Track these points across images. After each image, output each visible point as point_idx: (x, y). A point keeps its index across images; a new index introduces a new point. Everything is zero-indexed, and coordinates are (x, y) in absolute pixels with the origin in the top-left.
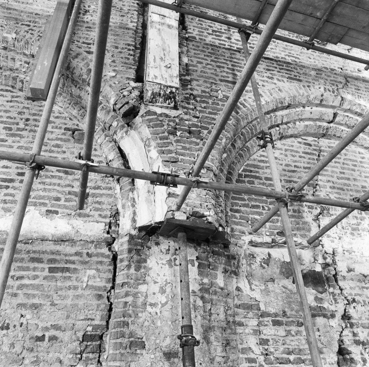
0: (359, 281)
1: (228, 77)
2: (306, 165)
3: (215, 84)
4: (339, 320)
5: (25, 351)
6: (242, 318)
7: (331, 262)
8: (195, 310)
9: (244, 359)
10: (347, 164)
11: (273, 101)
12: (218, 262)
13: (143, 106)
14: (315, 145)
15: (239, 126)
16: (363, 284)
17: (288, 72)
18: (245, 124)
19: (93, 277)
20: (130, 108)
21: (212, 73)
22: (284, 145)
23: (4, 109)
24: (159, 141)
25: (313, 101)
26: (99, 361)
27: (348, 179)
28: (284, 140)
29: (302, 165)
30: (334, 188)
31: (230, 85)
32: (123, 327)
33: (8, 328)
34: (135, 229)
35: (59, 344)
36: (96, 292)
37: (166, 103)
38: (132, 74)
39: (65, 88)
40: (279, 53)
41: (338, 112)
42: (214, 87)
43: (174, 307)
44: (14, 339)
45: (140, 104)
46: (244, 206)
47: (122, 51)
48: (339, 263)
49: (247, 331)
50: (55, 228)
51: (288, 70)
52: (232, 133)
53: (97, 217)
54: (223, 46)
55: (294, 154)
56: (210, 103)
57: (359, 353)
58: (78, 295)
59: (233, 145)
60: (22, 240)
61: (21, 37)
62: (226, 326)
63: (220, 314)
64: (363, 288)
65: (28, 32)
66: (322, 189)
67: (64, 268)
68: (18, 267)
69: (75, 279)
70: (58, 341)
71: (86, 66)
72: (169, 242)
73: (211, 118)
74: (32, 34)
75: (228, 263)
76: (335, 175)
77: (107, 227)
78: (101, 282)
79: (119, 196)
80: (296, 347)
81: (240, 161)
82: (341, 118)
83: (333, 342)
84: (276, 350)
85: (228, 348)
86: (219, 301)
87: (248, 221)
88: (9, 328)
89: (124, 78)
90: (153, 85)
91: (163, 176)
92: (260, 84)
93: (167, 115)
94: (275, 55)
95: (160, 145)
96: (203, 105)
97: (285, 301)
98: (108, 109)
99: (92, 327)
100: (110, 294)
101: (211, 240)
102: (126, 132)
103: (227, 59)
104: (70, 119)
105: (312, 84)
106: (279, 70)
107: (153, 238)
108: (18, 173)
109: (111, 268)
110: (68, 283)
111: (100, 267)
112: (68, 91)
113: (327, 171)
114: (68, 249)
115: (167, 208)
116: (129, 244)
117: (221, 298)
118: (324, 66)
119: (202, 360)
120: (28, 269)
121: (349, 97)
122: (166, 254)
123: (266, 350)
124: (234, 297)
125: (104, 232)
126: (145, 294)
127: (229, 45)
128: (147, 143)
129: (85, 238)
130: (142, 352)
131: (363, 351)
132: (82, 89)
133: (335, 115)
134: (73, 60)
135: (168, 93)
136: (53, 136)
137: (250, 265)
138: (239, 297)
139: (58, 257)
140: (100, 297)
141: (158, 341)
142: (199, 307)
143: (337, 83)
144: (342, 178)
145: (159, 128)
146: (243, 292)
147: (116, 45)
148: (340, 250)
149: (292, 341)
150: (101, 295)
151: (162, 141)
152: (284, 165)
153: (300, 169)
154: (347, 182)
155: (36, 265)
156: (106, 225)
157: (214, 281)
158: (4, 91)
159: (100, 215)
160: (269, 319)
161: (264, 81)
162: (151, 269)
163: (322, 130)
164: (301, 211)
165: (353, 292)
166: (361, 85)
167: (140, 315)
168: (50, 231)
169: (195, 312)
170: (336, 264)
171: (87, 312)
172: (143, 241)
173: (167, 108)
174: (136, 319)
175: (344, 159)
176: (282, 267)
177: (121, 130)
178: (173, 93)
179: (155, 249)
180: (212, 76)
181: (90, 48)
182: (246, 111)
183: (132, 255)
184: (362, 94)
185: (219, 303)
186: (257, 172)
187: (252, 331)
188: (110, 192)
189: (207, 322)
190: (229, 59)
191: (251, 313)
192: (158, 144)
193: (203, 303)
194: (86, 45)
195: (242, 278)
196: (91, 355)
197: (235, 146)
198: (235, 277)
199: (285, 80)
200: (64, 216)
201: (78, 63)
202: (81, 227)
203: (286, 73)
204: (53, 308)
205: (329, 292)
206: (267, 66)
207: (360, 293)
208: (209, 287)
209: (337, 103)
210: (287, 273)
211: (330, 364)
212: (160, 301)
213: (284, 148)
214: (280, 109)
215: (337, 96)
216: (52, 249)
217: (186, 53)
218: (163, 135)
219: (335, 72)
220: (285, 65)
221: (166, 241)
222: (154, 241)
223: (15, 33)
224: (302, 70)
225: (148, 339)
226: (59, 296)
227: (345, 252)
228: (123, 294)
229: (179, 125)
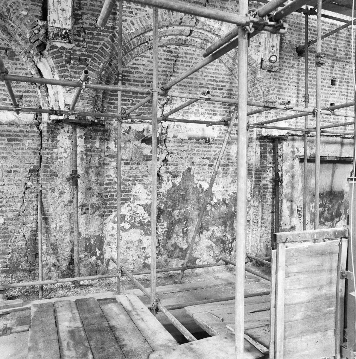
0: (179, 142)
2: (164, 69)
14: (175, 52)
16: (180, 144)
19: (31, 143)
24: (60, 69)
41: (194, 29)
52: (108, 58)
63: (96, 160)
75: (103, 135)
79: (40, 97)
82: (196, 34)
96: (90, 36)
102: (40, 59)
109: (40, 138)
110: (18, 147)
111: (33, 138)
133: (191, 32)
139: (11, 133)
140: (35, 153)
173: (64, 42)
176: (136, 134)
179: (61, 130)
186: (129, 76)
188: (35, 94)
192: (59, 71)
196: (34, 178)
209: (192, 24)
225: (59, 173)
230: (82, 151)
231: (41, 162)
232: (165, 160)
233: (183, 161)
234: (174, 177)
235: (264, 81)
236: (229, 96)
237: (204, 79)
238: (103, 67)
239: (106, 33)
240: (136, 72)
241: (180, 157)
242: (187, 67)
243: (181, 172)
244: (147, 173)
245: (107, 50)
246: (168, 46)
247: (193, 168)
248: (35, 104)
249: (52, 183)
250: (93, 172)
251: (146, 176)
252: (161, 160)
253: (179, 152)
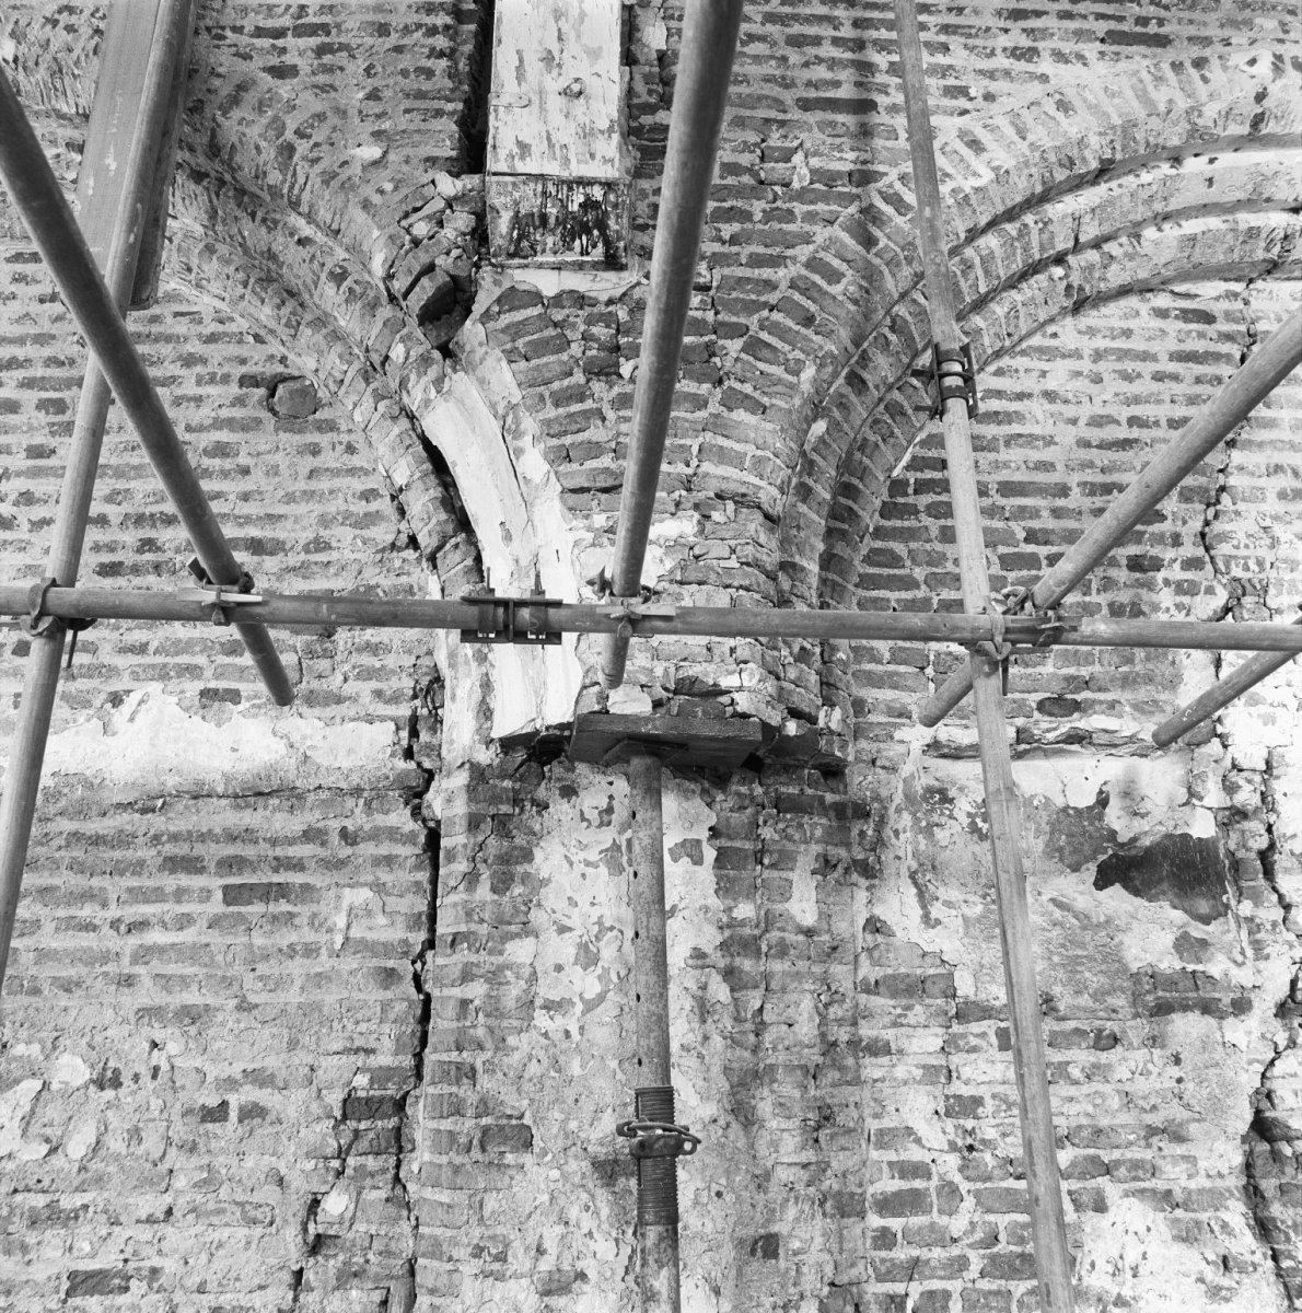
1: (837, 84)
3: (782, 124)
5: (173, 1152)
6: (884, 1027)
7: (1256, 800)
8: (702, 1014)
9: (885, 1167)
13: (486, 275)
15: (877, 298)
18: (904, 285)
19: (363, 909)
20: (439, 289)
21: (768, 79)
22: (1091, 332)
23: (32, 332)
24: (551, 412)
25: (1218, 131)
26: (397, 1179)
28: (1094, 313)
31: (841, 118)
32: (458, 1082)
33: (116, 1083)
34: (489, 742)
35: (270, 1130)
36: (375, 962)
37: (571, 249)
38: (444, 138)
39: (219, 228)
42: (775, 139)
43: (626, 1009)
44: (138, 1115)
45: (478, 266)
46: (911, 606)
47: (405, 41)
49: (900, 1072)
50: (234, 750)
52: (844, 334)
53: (367, 700)
56: (758, 216)
58: (319, 975)
59: (856, 381)
60: (131, 800)
61: (36, 50)
62: (820, 1060)
63: (798, 1020)
65: (55, 23)
66: (1241, 506)
67: (270, 885)
68: (130, 890)
69: (306, 921)
70: (268, 1119)
71: (271, 133)
72: (611, 783)
74: (70, 29)
77: (404, 734)
78: (391, 929)
80: (1084, 1121)
83: (1229, 1102)
84: (1004, 1135)
85: (823, 1135)
86: (798, 976)
87: (922, 669)
88: (121, 1084)
89: (416, 161)
90: (514, 184)
91: (501, 610)
93: (583, 297)
95: (556, 429)
96: (728, 230)
97: (1056, 959)
98: (372, 294)
99: (368, 1076)
100: (424, 964)
101: (768, 761)
102: (439, 382)
104: (258, 338)
107: (555, 769)
108: (102, 565)
109: (423, 876)
110: (287, 937)
111: (385, 876)
112: (231, 237)
113: (1270, 424)
114: (277, 821)
115: (581, 674)
116: (470, 800)
117: (802, 965)
119: (723, 1181)
120: (158, 895)
122: (601, 825)
123: (971, 1133)
125: (393, 755)
126: (527, 971)
128: (509, 420)
129: (332, 779)
130: (521, 1161)
132: (276, 222)
134: (224, 115)
136: (204, 414)
137: (928, 831)
138: (876, 954)
139: (249, 852)
140: (389, 976)
141: (573, 1125)
142: (718, 1006)
145: (552, 358)
146: (893, 935)
147: (381, 18)
149: (1071, 1099)
150: (393, 969)
151: (561, 411)
155: (184, 880)
156: (398, 729)
157: (778, 907)
158: (26, 261)
159: (378, 694)
160: (989, 1026)
161: (991, 75)
162: (544, 883)
163: (1263, 245)
164: (1145, 608)
167: (512, 1040)
168: (216, 763)
170: (1273, 810)
171: (350, 1026)
172: (517, 786)
173: (580, 266)
174: (499, 1054)
177: (419, 377)
179: (561, 809)
181: (283, 51)
182: (907, 227)
183: (480, 838)
185: (795, 984)
187: (918, 1073)
189: (747, 1054)
191: (918, 1009)
192: (547, 423)
194: (266, 42)
195: (892, 882)
196: (371, 1162)
197: (864, 382)
198: (863, 882)
199: (1091, 49)
200: (259, 707)
201: (242, 128)
202: (317, 740)
203: (1100, 16)
204: (246, 1020)
205: (1237, 917)
208: (757, 932)
210: (1075, 851)
211: (1209, 1176)
212: (578, 990)
213: (1088, 345)
214: (1065, 187)
216: (229, 823)
218: (566, 382)
221: (600, 779)
222: (559, 780)
223: (13, 35)
226: (261, 978)
228: (456, 972)
229: (627, 333)
230: (698, 954)
231: (424, 1042)
239: (820, 207)
240: (1010, 441)
244: (1176, 1112)
245: (836, 289)
246: (1178, 288)
248: (409, 661)
249: (491, 1203)
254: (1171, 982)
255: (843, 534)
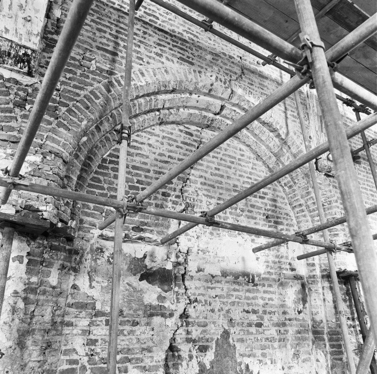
0: (206, 281)
1: (108, 46)
3: (91, 51)
4: (176, 319)
6: (73, 318)
7: (183, 261)
9: (65, 361)
10: (224, 160)
11: (155, 83)
12: (55, 258)
14: (196, 136)
15: (108, 107)
16: (209, 285)
17: (181, 51)
18: (116, 105)
21: (89, 37)
22: (163, 131)
25: (201, 90)
27: (222, 176)
29: (177, 156)
30: (205, 184)
31: (108, 55)
40: (177, 27)
41: (226, 105)
42: (88, 54)
46: (102, 195)
48: (190, 263)
49: (75, 332)
51: (182, 49)
52: (97, 114)
54: (112, 5)
55: (171, 142)
56: (78, 74)
57: (188, 350)
59: (98, 128)
62: (50, 327)
63: (46, 314)
64: (209, 288)
66: (191, 184)
73: (74, 93)
75: (68, 259)
76: (210, 171)
80: (126, 347)
81: (105, 146)
84: (103, 351)
92: (144, 60)
94: (172, 28)
96: (68, 75)
97: (125, 300)
103: (113, 22)
105: (205, 70)
106: (172, 47)
113: (202, 165)
117: (50, 298)
118: (223, 51)
119: (10, 367)
121: (239, 91)
123: (93, 350)
124: (67, 296)
127: (119, 5)
131: (192, 349)
133: (222, 108)
135: (21, 54)
137: (95, 260)
138: (74, 295)
143: (232, 74)
144: (216, 175)
145: (3, 97)
146: (80, 290)
148: (195, 250)
149: (123, 340)
152: (157, 154)
153: (174, 161)
154: (219, 179)
157: (45, 279)
160: (103, 319)
161: (150, 57)
164: (164, 206)
165: (197, 292)
166: (256, 80)
169: (13, 314)
173: (19, 72)
175: (223, 155)
176: (131, 263)
178: (28, 55)
180: (88, 40)
182: (120, 90)
184: (254, 90)
190: (115, 22)
191: (84, 312)
193: (25, 304)
197: (100, 129)
198: (73, 274)
199: (175, 60)
205: (174, 291)
206: (159, 39)
207: (204, 293)
208: (37, 286)
209: (226, 96)
210: (136, 270)
213: (162, 134)
215: (228, 88)
217: (60, 4)
218: (6, 106)
219: (233, 60)
220: (180, 42)
224: (198, 51)
227: (199, 252)
229: (30, 96)
230: (16, 292)
232: (184, 316)
233: (215, 316)
234: (201, 351)
235: (323, 187)
236: (273, 208)
237: (239, 180)
238: (87, 128)
239: (97, 77)
240: (137, 154)
241: (209, 308)
242: (214, 160)
243: (212, 339)
244: (150, 344)
247: (232, 331)
250: (35, 343)
251: (149, 350)
252: (177, 315)
253: (209, 300)
254: (154, 308)
255: (86, 171)
